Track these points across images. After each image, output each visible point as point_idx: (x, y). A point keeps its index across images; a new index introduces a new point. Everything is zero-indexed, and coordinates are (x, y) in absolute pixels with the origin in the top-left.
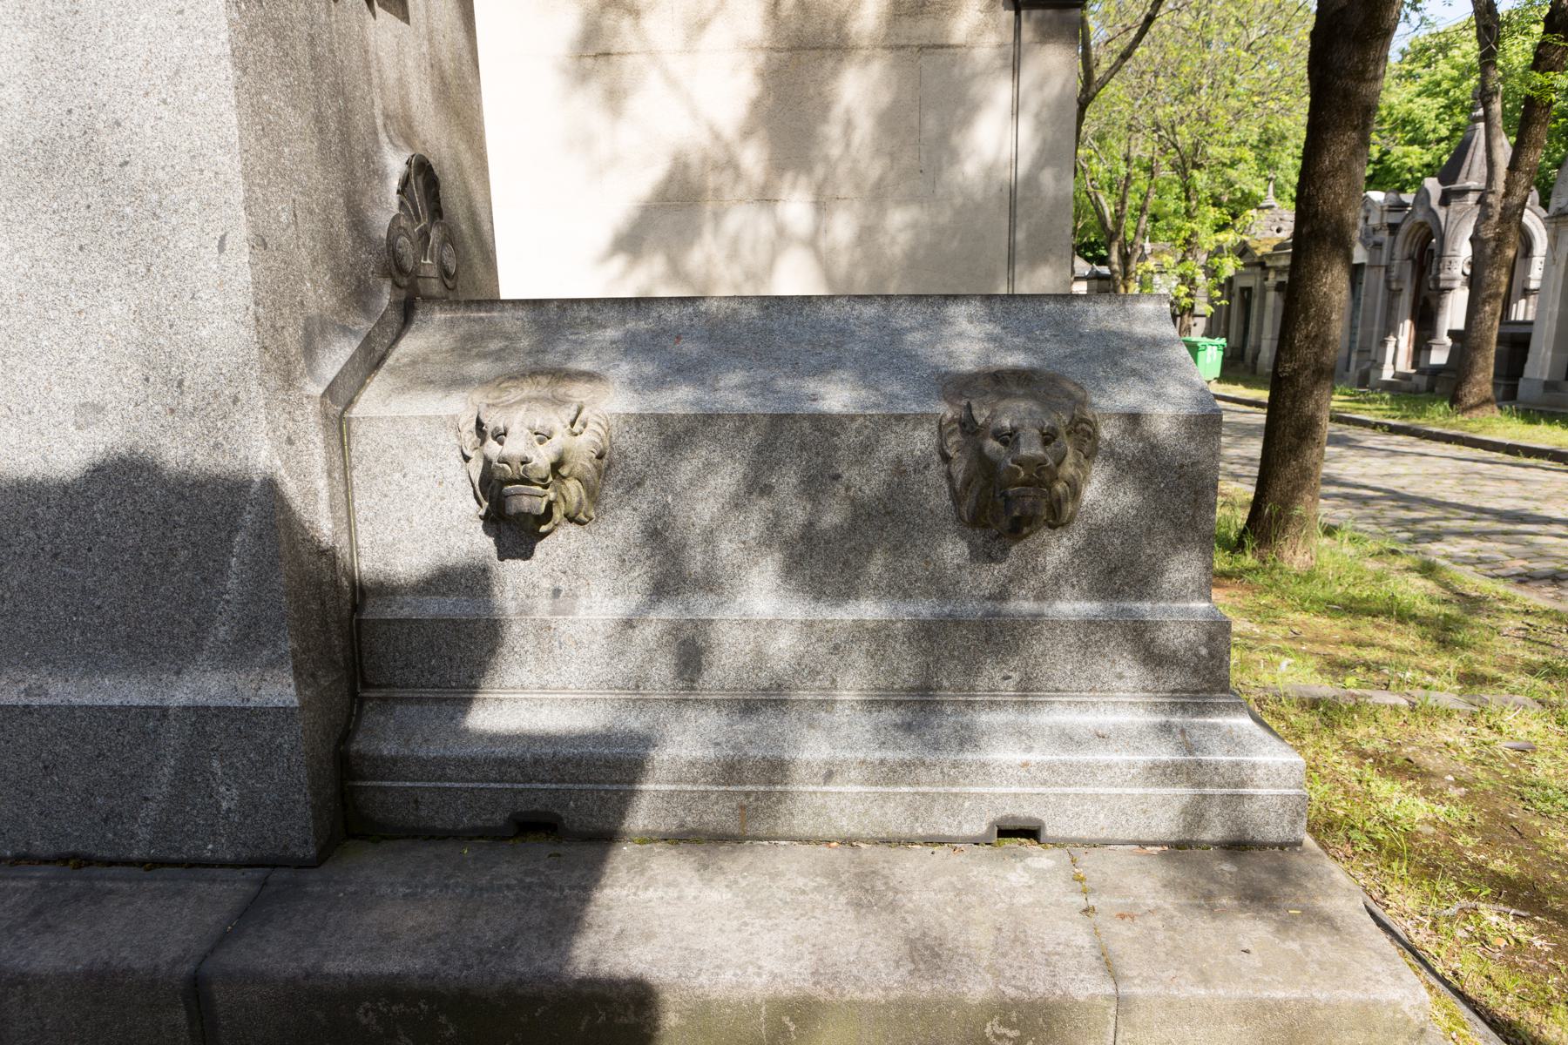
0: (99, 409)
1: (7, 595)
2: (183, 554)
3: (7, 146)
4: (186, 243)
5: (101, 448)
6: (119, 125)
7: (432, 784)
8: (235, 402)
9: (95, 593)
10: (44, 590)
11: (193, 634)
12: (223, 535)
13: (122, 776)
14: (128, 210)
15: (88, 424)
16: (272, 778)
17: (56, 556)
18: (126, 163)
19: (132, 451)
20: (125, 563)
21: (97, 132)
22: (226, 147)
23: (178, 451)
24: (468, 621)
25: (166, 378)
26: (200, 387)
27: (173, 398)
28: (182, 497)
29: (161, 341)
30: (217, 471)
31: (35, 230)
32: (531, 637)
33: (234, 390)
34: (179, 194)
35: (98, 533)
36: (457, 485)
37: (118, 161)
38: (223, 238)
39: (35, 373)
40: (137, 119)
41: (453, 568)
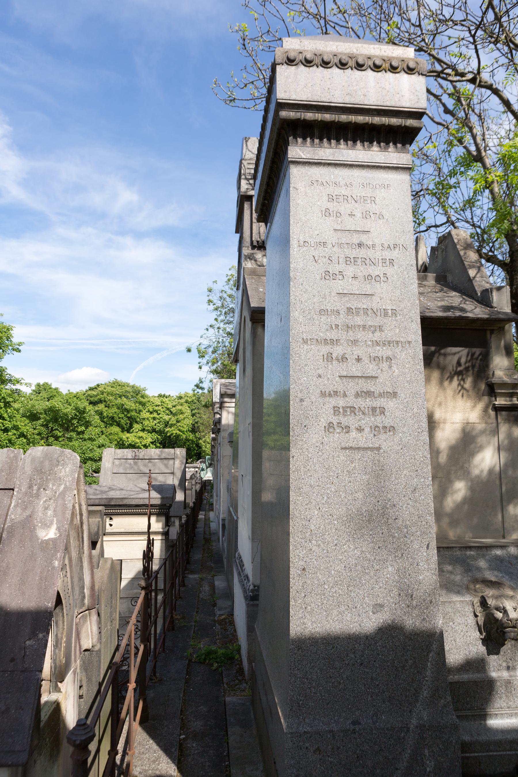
0: (381, 606)
1: (342, 681)
2: (410, 662)
3: (356, 512)
4: (416, 546)
5: (382, 621)
6: (395, 506)
7: (485, 754)
8: (431, 603)
9: (376, 679)
10: (356, 679)
11: (414, 694)
12: (425, 653)
13: (388, 759)
14: (396, 534)
15: (377, 612)
16: (448, 756)
17: (361, 664)
18: (396, 519)
19: (393, 622)
20: (388, 666)
21: (387, 508)
22: (430, 515)
23: (411, 622)
24: (481, 681)
25: (406, 593)
26: (419, 597)
27: (409, 601)
28: (411, 639)
29: (406, 580)
30: (424, 629)
31: (363, 541)
32: (504, 687)
33: (431, 598)
34: (414, 529)
35: (378, 654)
36: (472, 626)
37: (394, 518)
38: (428, 544)
39: (359, 593)
40: (401, 504)
41: (471, 659)
